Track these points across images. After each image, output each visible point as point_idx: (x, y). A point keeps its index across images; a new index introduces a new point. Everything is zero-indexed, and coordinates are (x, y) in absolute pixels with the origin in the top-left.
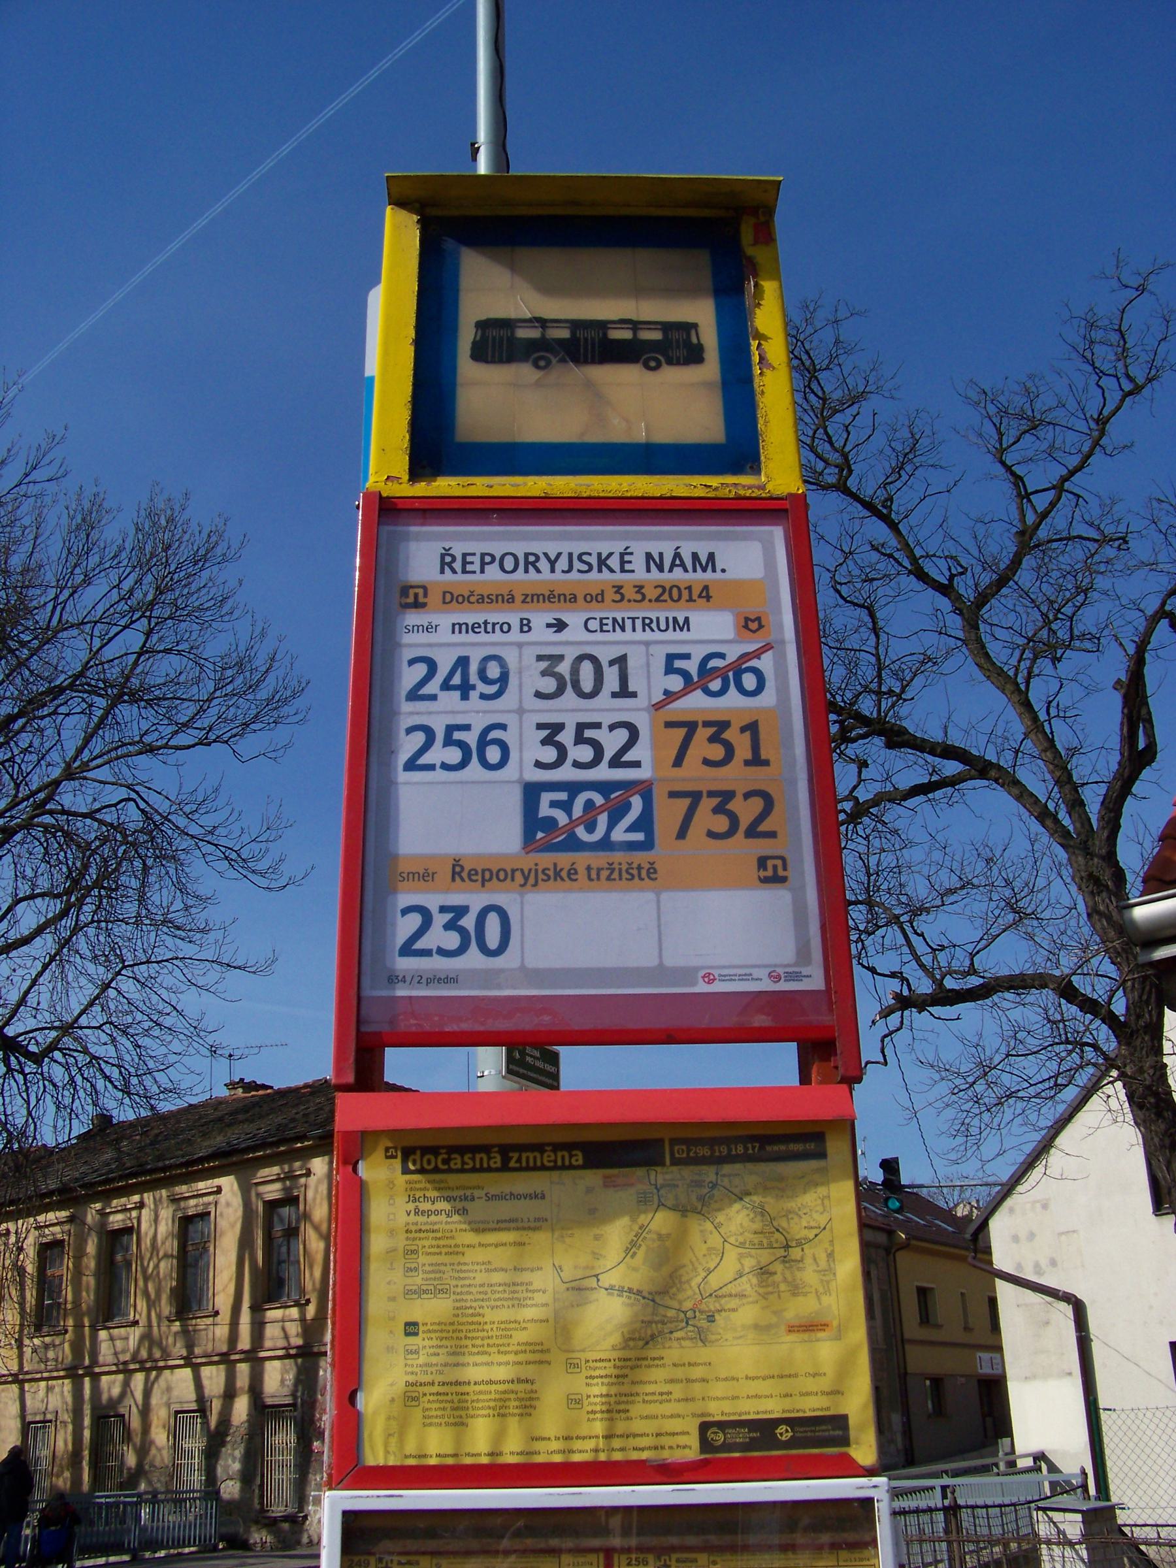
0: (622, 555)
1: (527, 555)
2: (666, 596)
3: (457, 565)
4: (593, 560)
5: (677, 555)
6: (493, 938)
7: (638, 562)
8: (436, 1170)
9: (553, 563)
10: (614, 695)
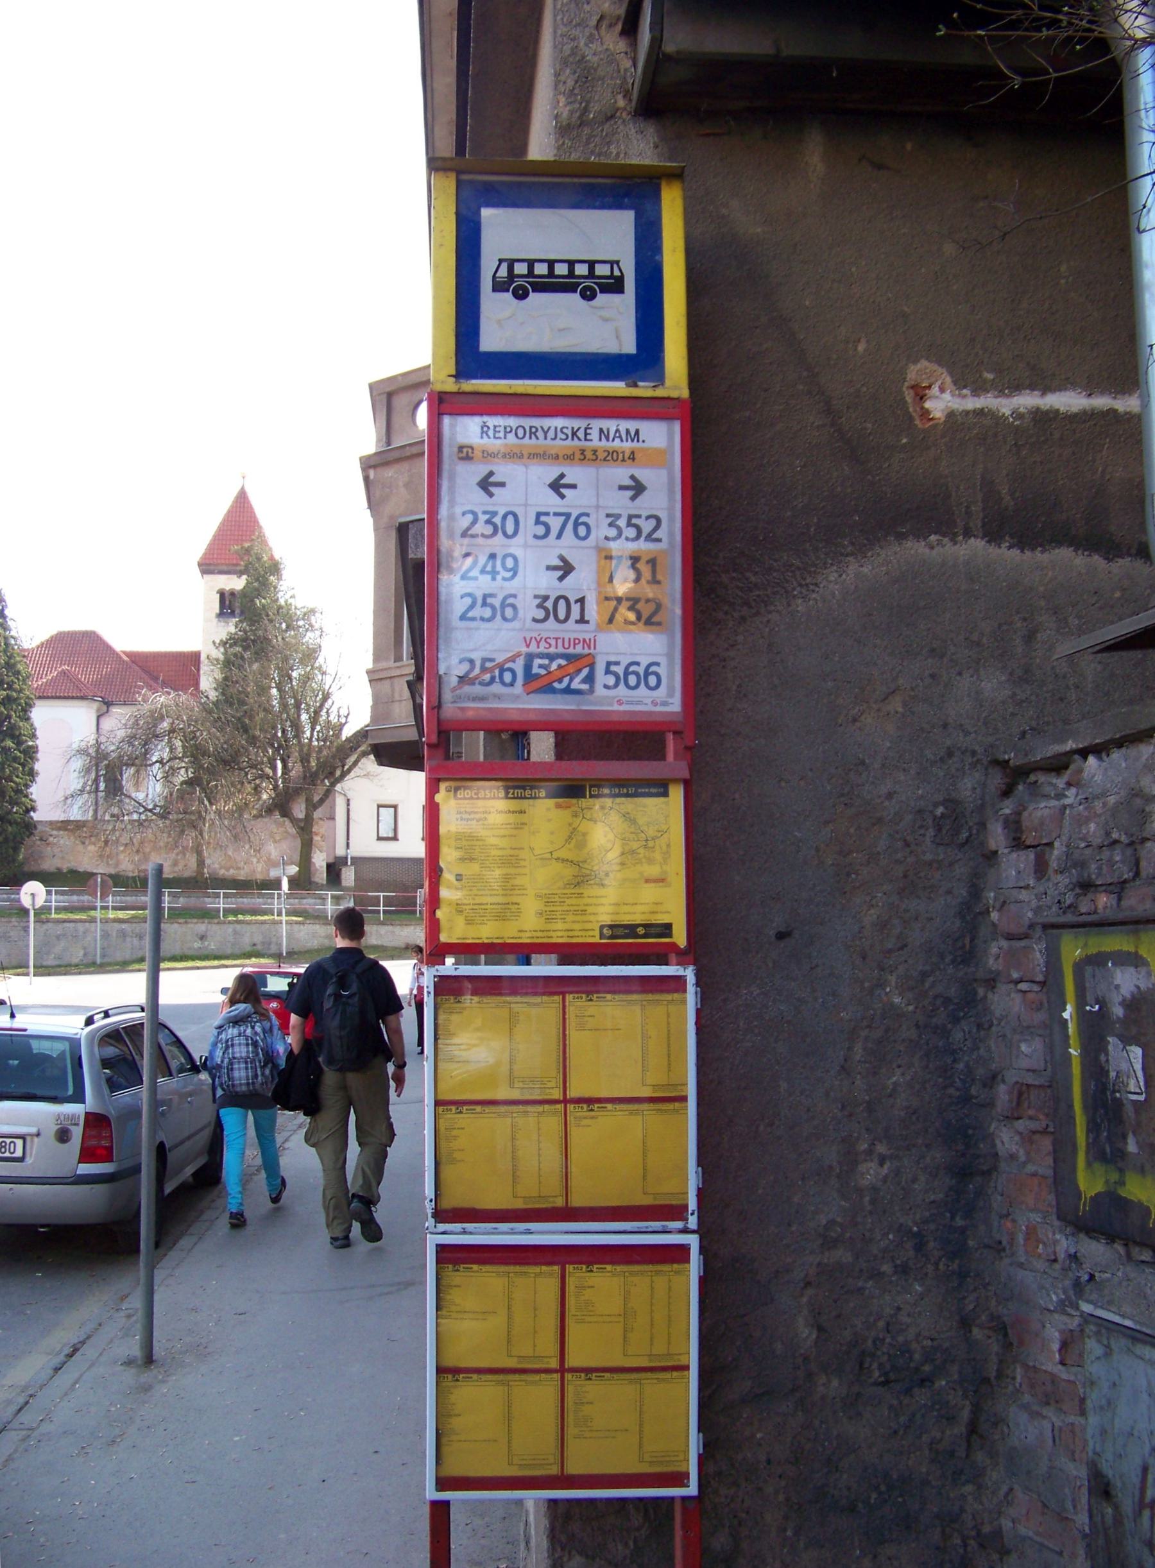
0: (586, 429)
1: (531, 428)
2: (609, 458)
3: (491, 433)
4: (569, 433)
5: (617, 431)
6: (510, 529)
7: (594, 434)
8: (471, 798)
9: (546, 433)
10: (577, 622)
